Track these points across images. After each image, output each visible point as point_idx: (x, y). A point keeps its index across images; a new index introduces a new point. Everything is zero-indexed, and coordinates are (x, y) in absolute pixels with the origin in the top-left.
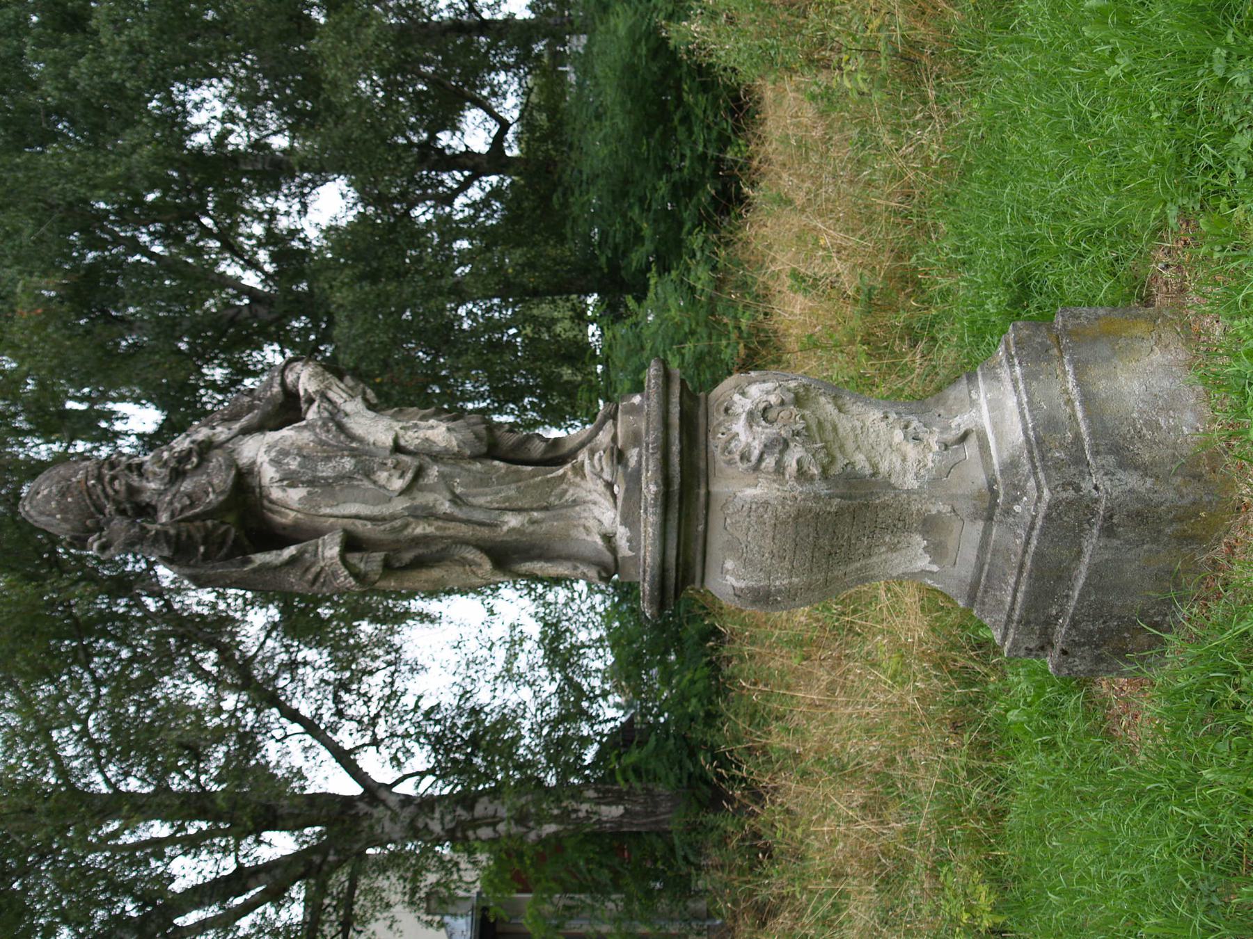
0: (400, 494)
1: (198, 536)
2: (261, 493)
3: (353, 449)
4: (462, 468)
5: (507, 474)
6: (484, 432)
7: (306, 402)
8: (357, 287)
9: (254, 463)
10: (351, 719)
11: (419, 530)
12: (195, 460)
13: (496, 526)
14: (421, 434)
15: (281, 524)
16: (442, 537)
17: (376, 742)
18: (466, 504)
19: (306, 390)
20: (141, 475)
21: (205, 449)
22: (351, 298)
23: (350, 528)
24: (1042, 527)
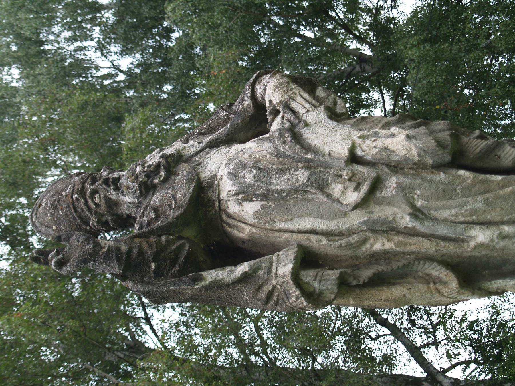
0: (355, 208)
1: (149, 253)
2: (220, 206)
3: (308, 161)
4: (423, 178)
5: (473, 184)
6: (448, 139)
7: (271, 113)
8: (422, 47)
9: (215, 176)
10: (419, 328)
11: (378, 246)
12: (162, 174)
13: (463, 241)
14: (380, 143)
15: (238, 238)
16: (404, 253)
17: (436, 344)
18: (429, 218)
19: (271, 102)
20: (117, 189)
21: (172, 163)
22: (417, 54)
23: (306, 243)
24: (81, 41)
